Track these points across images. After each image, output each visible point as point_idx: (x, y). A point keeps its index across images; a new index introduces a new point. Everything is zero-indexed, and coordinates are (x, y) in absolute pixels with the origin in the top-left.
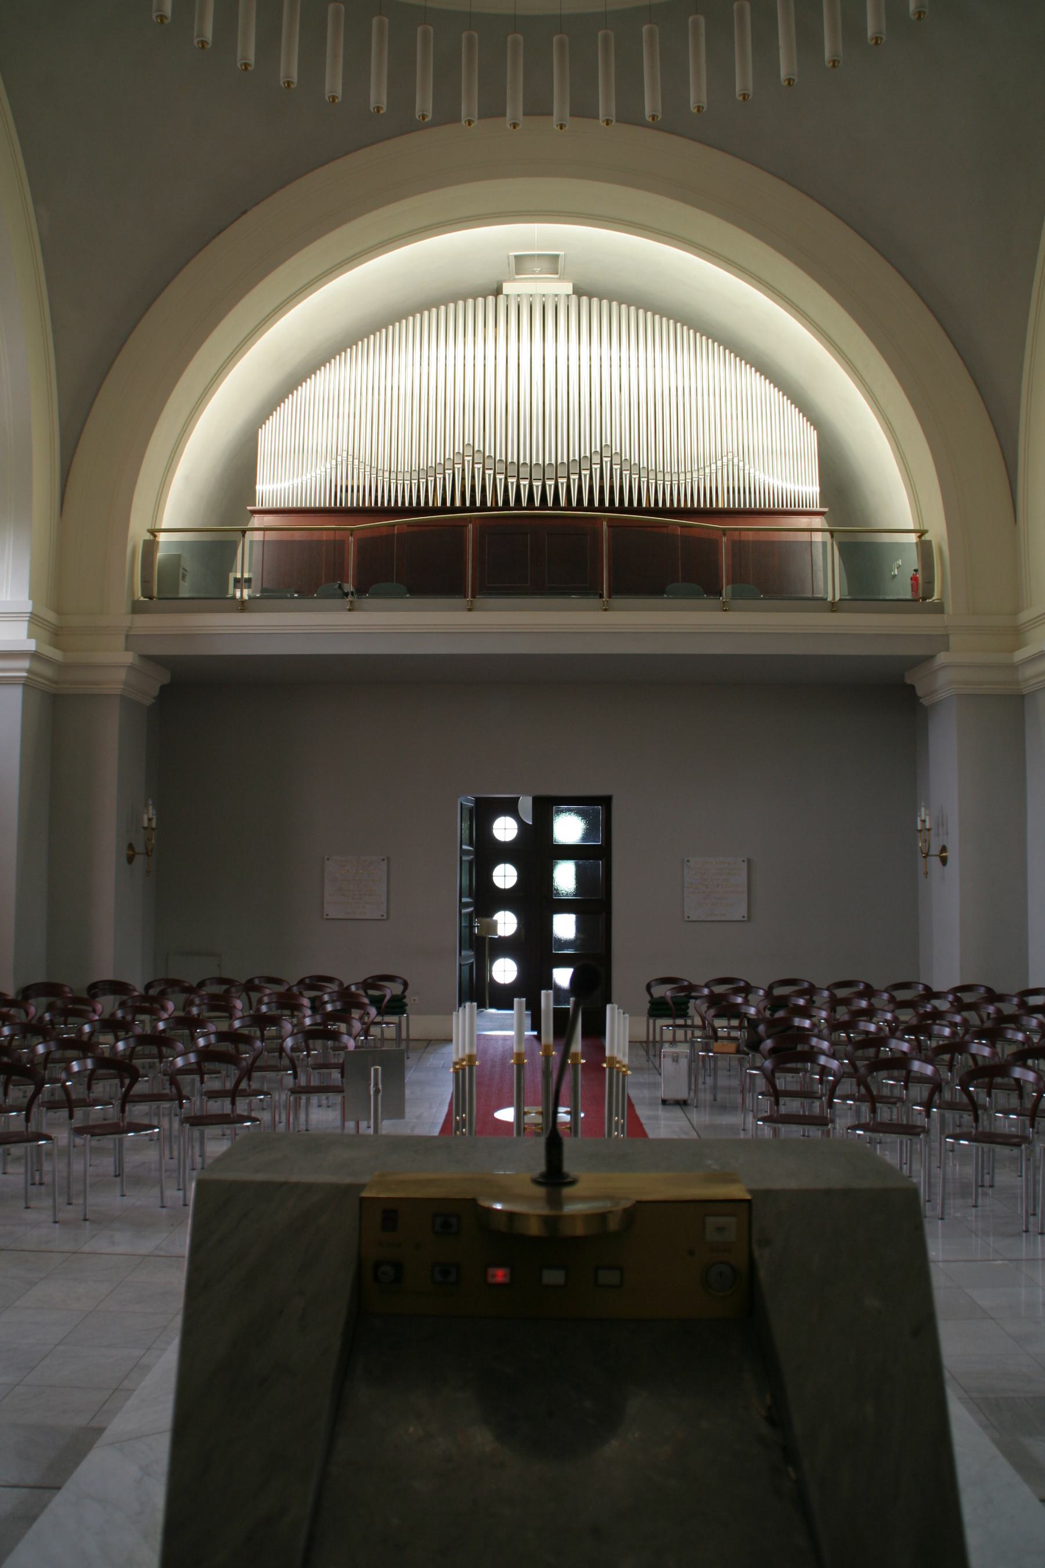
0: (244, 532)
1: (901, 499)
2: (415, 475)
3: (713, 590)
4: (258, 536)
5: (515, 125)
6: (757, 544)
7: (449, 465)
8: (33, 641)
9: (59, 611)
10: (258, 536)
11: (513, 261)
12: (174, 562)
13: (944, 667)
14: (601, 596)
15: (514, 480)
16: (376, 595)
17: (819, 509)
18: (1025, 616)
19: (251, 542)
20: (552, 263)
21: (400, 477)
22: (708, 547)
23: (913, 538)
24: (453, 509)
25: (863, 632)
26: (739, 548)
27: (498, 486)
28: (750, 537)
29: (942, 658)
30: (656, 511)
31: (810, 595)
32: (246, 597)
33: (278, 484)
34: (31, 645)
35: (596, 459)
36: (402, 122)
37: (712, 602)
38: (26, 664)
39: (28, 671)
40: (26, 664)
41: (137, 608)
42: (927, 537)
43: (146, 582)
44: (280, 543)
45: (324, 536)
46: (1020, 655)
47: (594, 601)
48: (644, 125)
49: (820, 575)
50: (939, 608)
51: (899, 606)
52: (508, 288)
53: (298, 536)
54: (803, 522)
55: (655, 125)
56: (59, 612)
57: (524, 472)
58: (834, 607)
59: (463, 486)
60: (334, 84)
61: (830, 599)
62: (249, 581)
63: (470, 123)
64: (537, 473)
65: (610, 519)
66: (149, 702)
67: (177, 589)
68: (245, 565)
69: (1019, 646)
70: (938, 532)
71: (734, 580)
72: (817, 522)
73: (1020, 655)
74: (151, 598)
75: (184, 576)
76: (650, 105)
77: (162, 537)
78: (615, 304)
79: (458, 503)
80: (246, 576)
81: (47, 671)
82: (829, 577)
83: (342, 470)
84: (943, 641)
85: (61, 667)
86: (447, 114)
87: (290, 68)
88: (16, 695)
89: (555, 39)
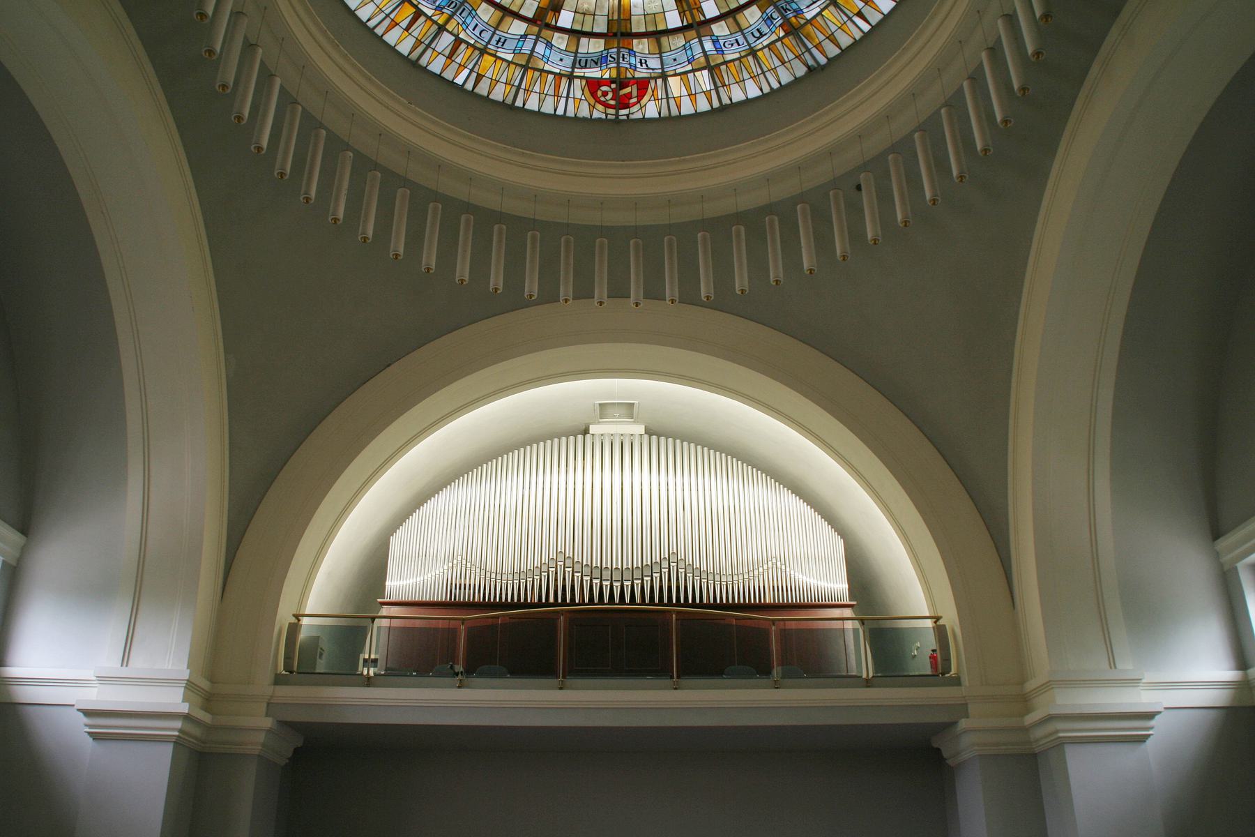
0: (373, 619)
1: (917, 590)
2: (517, 577)
3: (765, 671)
4: (385, 623)
5: (601, 303)
6: (799, 631)
7: (544, 568)
8: (187, 705)
9: (212, 679)
10: (385, 623)
11: (597, 407)
12: (314, 642)
13: (965, 731)
14: (672, 677)
15: (598, 581)
16: (481, 675)
17: (848, 602)
18: (1031, 685)
19: (379, 628)
20: (629, 410)
21: (504, 577)
22: (761, 635)
23: (929, 623)
24: (547, 604)
25: (892, 703)
26: (785, 635)
27: (584, 586)
28: (793, 625)
29: (963, 724)
30: (715, 606)
31: (844, 674)
32: (371, 673)
33: (403, 581)
34: (184, 708)
35: (665, 564)
36: (514, 301)
37: (764, 681)
38: (178, 724)
39: (180, 731)
40: (178, 724)
41: (278, 680)
42: (941, 622)
43: (288, 658)
44: (404, 630)
45: (441, 624)
46: (1030, 719)
47: (668, 682)
48: (702, 305)
49: (852, 657)
50: (957, 681)
51: (920, 681)
52: (593, 429)
53: (418, 623)
54: (836, 613)
55: (711, 305)
56: (212, 684)
57: (606, 575)
58: (868, 683)
59: (556, 586)
60: (463, 270)
61: (864, 676)
62: (375, 661)
63: (566, 301)
64: (617, 576)
65: (678, 613)
66: (283, 762)
67: (314, 665)
68: (374, 648)
69: (1028, 710)
70: (950, 618)
71: (782, 663)
72: (848, 613)
73: (1030, 719)
74: (291, 672)
75: (321, 655)
76: (705, 289)
77: (305, 621)
78: (678, 441)
79: (551, 600)
80: (373, 657)
81: (196, 731)
82: (858, 657)
83: (457, 570)
84: (962, 709)
85: (209, 728)
86: (549, 296)
87: (430, 258)
88: (167, 751)
89: (632, 242)
